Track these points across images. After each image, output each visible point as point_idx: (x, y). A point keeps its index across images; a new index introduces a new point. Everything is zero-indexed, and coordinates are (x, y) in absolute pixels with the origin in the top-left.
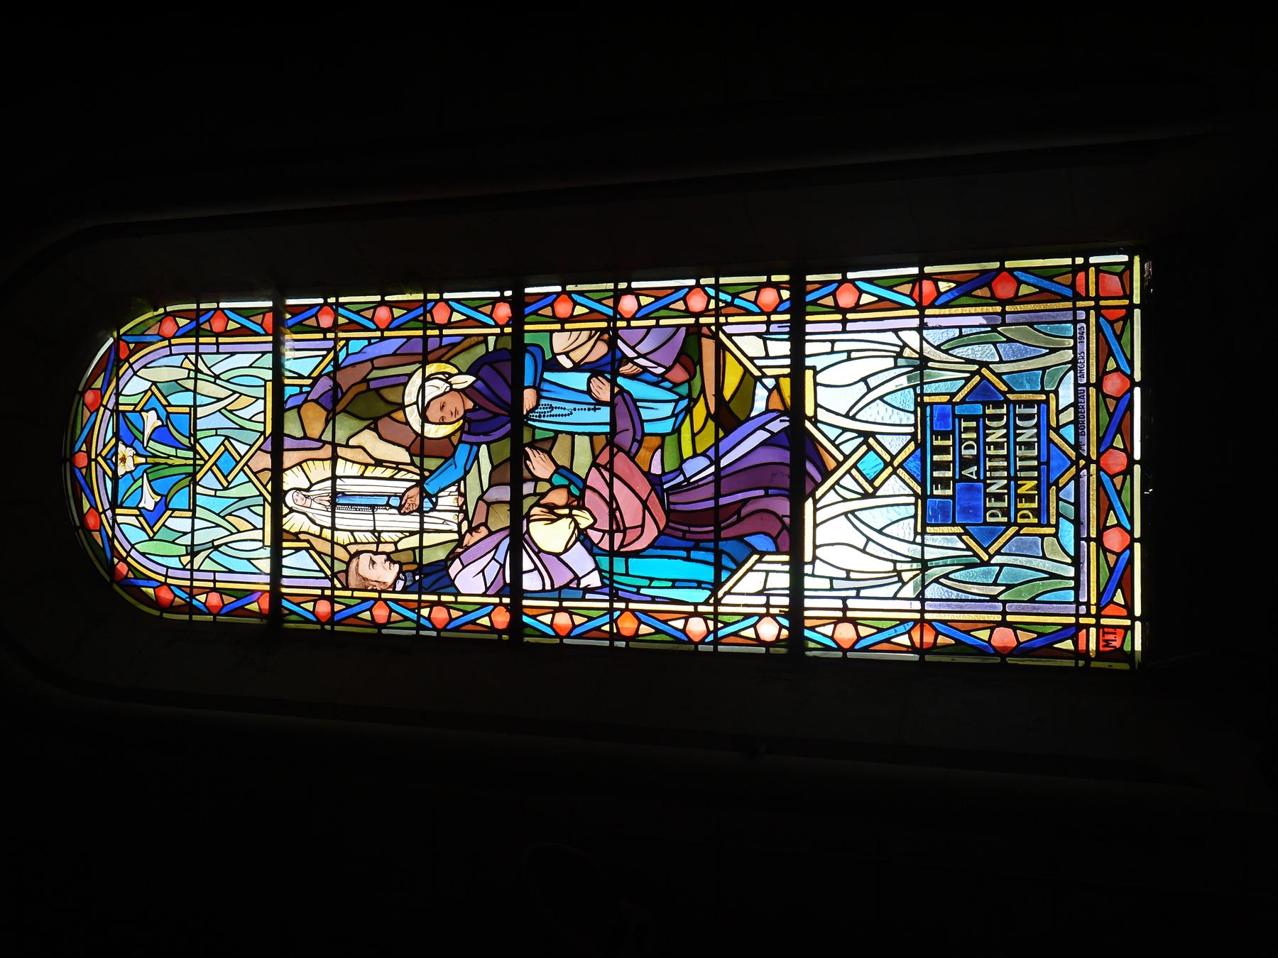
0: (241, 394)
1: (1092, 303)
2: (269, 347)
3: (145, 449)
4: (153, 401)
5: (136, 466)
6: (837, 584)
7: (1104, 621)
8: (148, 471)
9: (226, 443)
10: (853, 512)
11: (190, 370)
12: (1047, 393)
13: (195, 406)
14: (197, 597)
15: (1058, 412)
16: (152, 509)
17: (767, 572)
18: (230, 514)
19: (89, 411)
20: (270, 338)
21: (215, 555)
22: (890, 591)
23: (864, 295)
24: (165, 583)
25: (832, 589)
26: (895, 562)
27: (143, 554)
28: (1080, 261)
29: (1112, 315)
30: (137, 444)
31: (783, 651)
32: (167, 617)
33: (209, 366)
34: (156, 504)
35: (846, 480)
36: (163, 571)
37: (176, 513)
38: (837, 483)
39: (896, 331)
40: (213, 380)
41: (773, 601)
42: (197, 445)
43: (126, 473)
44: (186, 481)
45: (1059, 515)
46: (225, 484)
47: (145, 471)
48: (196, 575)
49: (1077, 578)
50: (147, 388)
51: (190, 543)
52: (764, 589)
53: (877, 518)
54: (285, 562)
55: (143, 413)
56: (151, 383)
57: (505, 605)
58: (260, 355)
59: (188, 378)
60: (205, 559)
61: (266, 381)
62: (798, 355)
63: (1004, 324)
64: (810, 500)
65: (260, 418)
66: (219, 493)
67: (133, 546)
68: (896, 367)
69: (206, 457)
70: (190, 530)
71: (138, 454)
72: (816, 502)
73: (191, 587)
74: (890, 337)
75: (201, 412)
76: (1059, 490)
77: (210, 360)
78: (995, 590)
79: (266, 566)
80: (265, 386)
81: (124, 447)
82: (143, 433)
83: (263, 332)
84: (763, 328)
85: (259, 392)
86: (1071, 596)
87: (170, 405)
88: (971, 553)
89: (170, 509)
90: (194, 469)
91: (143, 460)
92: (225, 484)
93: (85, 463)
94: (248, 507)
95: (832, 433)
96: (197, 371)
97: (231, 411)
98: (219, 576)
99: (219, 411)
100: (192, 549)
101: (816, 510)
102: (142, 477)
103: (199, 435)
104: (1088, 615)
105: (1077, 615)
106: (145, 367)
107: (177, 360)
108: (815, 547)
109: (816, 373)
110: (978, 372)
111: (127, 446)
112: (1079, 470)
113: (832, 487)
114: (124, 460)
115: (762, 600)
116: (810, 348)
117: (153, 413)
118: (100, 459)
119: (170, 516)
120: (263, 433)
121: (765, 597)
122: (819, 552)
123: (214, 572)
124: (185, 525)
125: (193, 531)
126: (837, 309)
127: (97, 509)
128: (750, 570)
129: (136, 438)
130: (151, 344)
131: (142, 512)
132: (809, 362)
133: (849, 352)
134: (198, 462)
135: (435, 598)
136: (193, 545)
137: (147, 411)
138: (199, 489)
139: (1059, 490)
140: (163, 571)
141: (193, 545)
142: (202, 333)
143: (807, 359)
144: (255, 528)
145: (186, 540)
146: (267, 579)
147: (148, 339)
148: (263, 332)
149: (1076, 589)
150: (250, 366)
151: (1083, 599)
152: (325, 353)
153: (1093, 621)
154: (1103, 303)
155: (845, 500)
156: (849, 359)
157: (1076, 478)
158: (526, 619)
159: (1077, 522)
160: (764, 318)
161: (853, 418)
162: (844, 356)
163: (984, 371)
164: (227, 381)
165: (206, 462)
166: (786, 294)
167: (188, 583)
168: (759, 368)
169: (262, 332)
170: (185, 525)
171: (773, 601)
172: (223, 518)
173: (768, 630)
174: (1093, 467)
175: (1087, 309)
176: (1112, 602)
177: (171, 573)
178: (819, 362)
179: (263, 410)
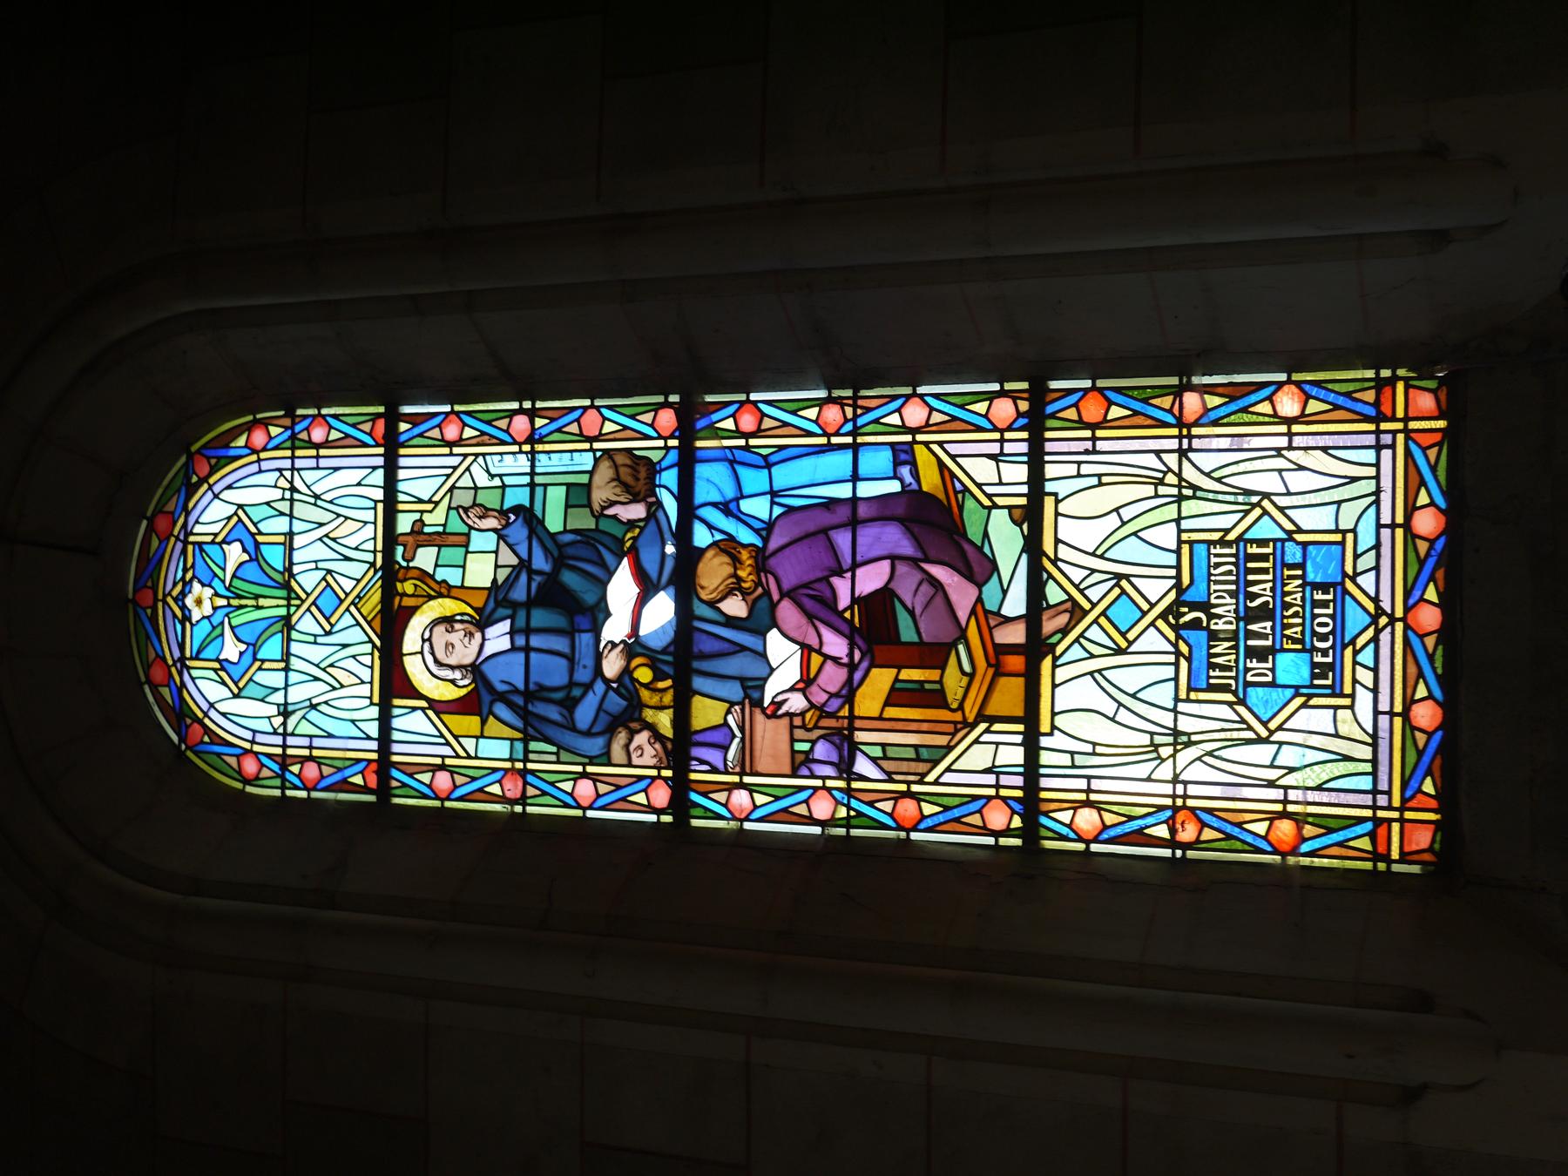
0: (347, 518)
1: (1400, 426)
2: (380, 461)
3: (228, 589)
4: (240, 530)
5: (215, 609)
6: (1079, 760)
7: (1409, 815)
8: (231, 616)
9: (329, 578)
10: (1099, 671)
11: (284, 489)
12: (1344, 532)
13: (290, 535)
14: (290, 768)
15: (1356, 556)
16: (236, 661)
17: (998, 744)
18: (331, 665)
19: (159, 539)
20: (381, 450)
21: (313, 715)
22: (1143, 770)
23: (1113, 407)
24: (250, 751)
25: (1074, 766)
26: (1152, 734)
27: (224, 715)
28: (1386, 373)
29: (1426, 440)
30: (216, 583)
31: (1017, 842)
32: (291, 795)
33: (1000, 746)
34: (241, 654)
35: (1095, 633)
36: (248, 735)
37: (266, 665)
38: (1082, 635)
39: (1158, 453)
40: (312, 500)
41: (1004, 780)
42: (292, 580)
43: (204, 617)
44: (278, 626)
45: (1355, 681)
46: (328, 628)
47: (227, 615)
48: (291, 741)
49: (1374, 761)
50: (233, 512)
51: (283, 702)
52: (994, 766)
53: (1129, 679)
54: (396, 723)
55: (224, 546)
56: (236, 507)
57: (665, 779)
58: (371, 470)
59: (283, 499)
60: (300, 720)
61: (376, 502)
62: (1036, 480)
63: (1290, 448)
64: (1049, 659)
65: (370, 546)
66: (320, 640)
67: (212, 705)
68: (1157, 496)
69: (303, 596)
70: (283, 686)
71: (217, 594)
72: (1055, 659)
73: (284, 755)
74: (1151, 461)
75: (298, 541)
76: (1356, 653)
77: (310, 476)
78: (1272, 774)
79: (373, 729)
80: (375, 508)
81: (199, 585)
82: (224, 570)
83: (372, 442)
84: (994, 448)
85: (369, 515)
86: (1366, 783)
87: (260, 533)
88: (1245, 726)
89: (260, 660)
90: (288, 611)
91: (223, 602)
92: (328, 628)
93: (150, 602)
94: (354, 657)
95: (1077, 575)
96: (293, 489)
97: (334, 540)
98: (317, 743)
99: (320, 539)
100: (285, 708)
101: (1054, 667)
102: (222, 623)
103: (296, 569)
104: (1390, 808)
105: (1375, 807)
106: (229, 487)
107: (270, 478)
108: (1054, 714)
109: (1057, 502)
110: (1258, 504)
111: (203, 585)
112: (1378, 631)
113: (1077, 640)
114: (199, 602)
115: (991, 779)
116: (1050, 471)
117: (237, 545)
118: (169, 600)
119: (260, 669)
120: (373, 564)
121: (994, 776)
122: (1059, 721)
123: (311, 737)
124: (277, 679)
125: (287, 686)
126: (1081, 424)
127: (164, 659)
128: (976, 741)
129: (215, 575)
130: (241, 457)
131: (223, 665)
132: (1049, 487)
133: (1100, 476)
134: (293, 602)
135: (1003, 841)
136: (286, 704)
137: (229, 543)
138: (294, 635)
139: (1356, 653)
140: (248, 735)
141: (286, 704)
142: (298, 443)
143: (1047, 483)
144: (363, 682)
145: (278, 697)
146: (374, 745)
147: (232, 453)
148: (372, 442)
149: (1374, 774)
150: (359, 484)
151: (1383, 786)
152: (450, 471)
153: (1396, 815)
154: (1413, 425)
155: (1092, 656)
156: (1101, 484)
157: (1375, 640)
158: (694, 797)
159: (1375, 691)
160: (997, 436)
161: (1102, 557)
162: (1095, 481)
163: (1266, 503)
164: (331, 502)
165: (303, 601)
166: (1024, 406)
167: (279, 751)
168: (989, 496)
169: (371, 442)
170: (277, 679)
171: (1004, 780)
172: (324, 670)
173: (998, 817)
174: (1399, 626)
175: (1394, 433)
176: (1419, 791)
177: (259, 738)
178: (1062, 488)
179: (373, 536)
